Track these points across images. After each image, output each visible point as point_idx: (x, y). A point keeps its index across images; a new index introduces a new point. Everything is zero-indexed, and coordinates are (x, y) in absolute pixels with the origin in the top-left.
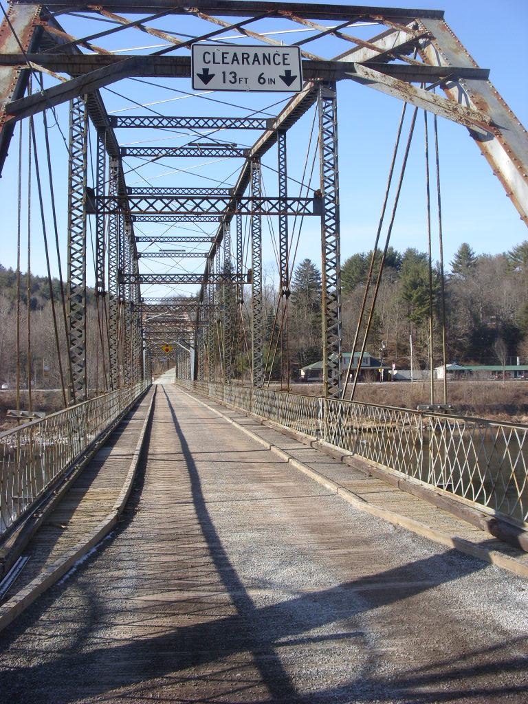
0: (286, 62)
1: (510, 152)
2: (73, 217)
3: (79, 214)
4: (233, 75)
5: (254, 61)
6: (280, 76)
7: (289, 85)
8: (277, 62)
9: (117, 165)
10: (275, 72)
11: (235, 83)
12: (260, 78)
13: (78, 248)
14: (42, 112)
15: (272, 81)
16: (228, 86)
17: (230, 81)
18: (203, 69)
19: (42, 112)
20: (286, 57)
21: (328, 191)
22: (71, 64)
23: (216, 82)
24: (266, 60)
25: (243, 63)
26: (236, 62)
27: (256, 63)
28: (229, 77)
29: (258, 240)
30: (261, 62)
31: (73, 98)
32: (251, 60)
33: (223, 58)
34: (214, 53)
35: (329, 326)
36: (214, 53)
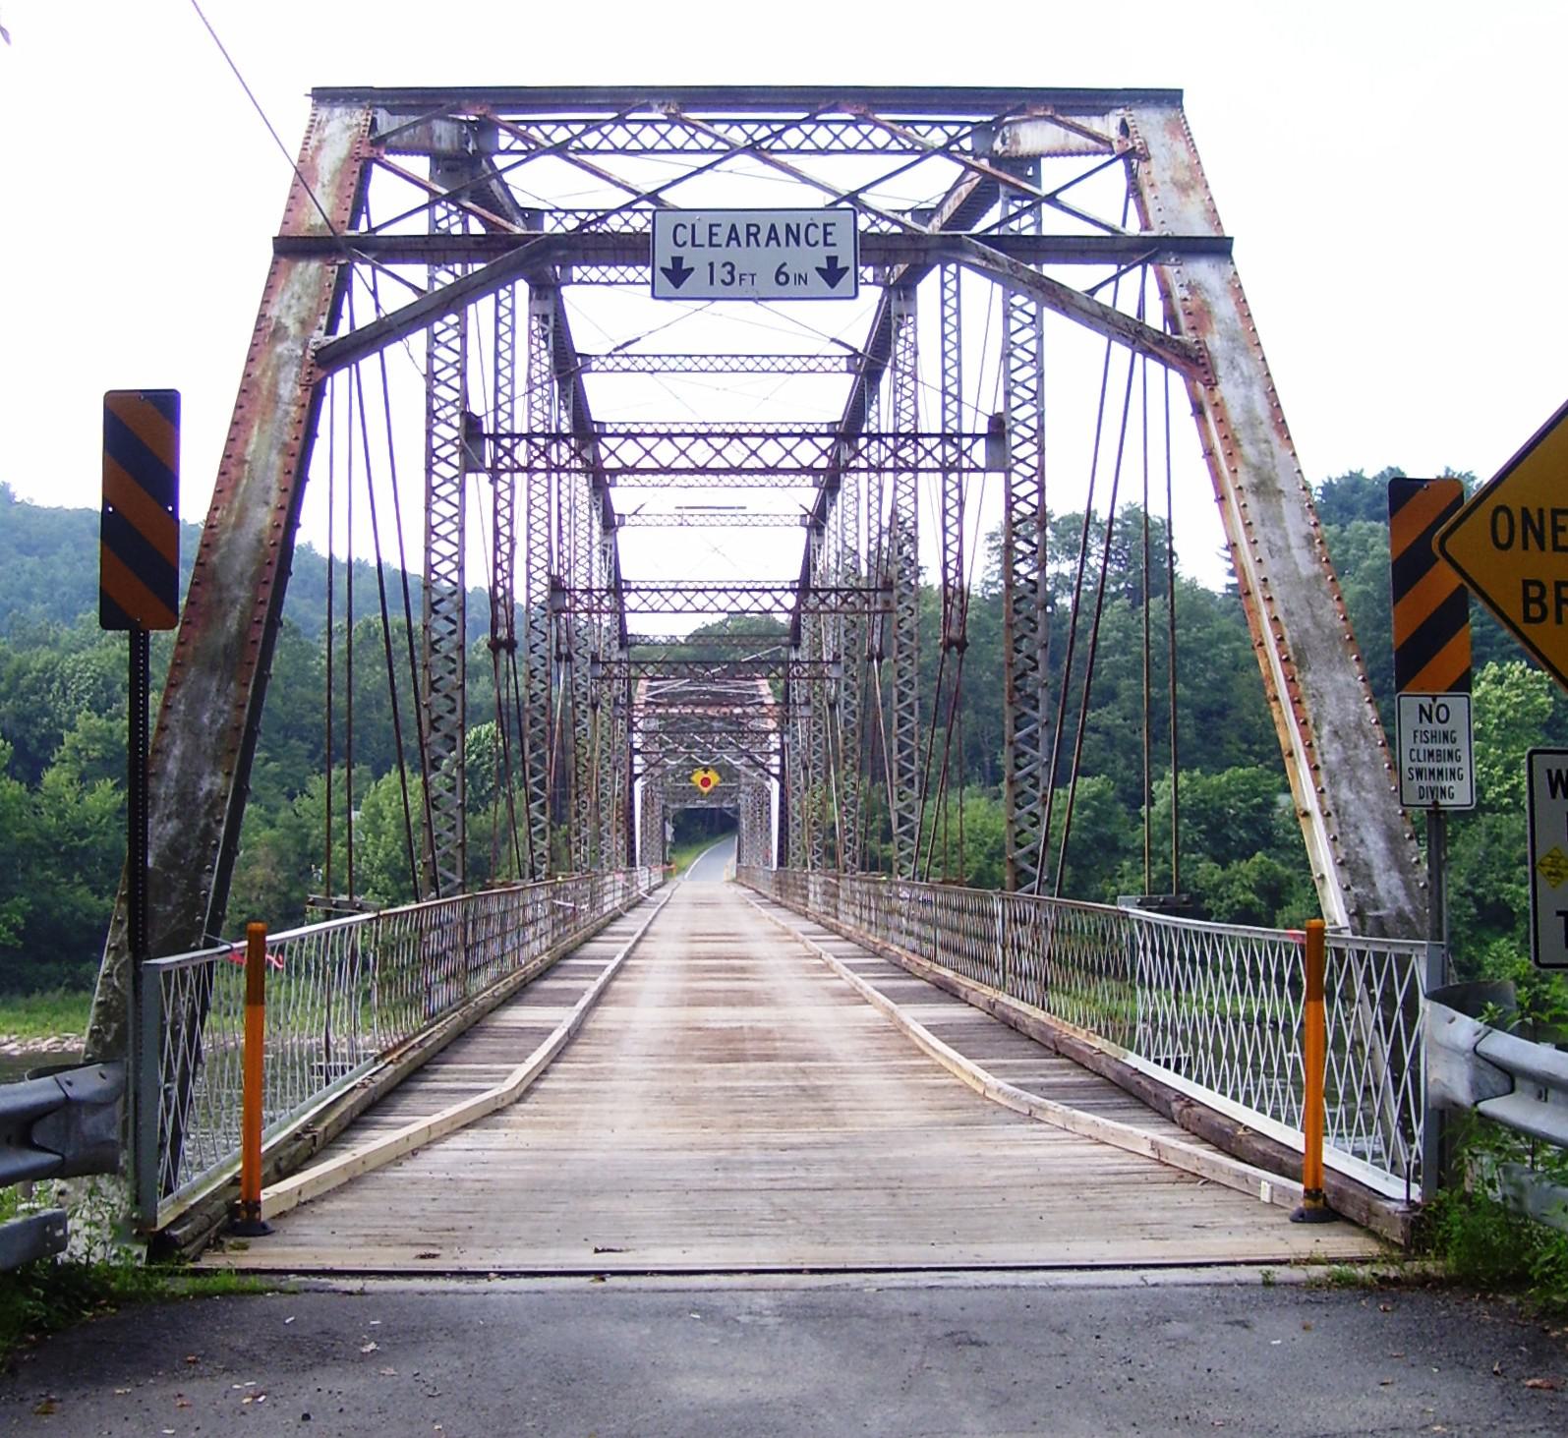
0: (830, 239)
1: (1221, 421)
2: (436, 481)
3: (449, 472)
4: (729, 268)
5: (769, 238)
6: (818, 269)
7: (832, 286)
8: (812, 242)
9: (549, 310)
10: (807, 259)
11: (731, 284)
12: (779, 272)
13: (449, 511)
14: (378, 355)
15: (802, 279)
16: (719, 289)
17: (723, 281)
18: (673, 258)
19: (378, 355)
20: (829, 229)
21: (1020, 414)
22: (429, 250)
23: (695, 282)
24: (791, 239)
25: (748, 244)
26: (733, 243)
27: (773, 243)
28: (721, 273)
29: (909, 500)
30: (783, 241)
31: (432, 324)
32: (763, 237)
33: (711, 234)
34: (693, 226)
35: (1018, 729)
36: (693, 226)
